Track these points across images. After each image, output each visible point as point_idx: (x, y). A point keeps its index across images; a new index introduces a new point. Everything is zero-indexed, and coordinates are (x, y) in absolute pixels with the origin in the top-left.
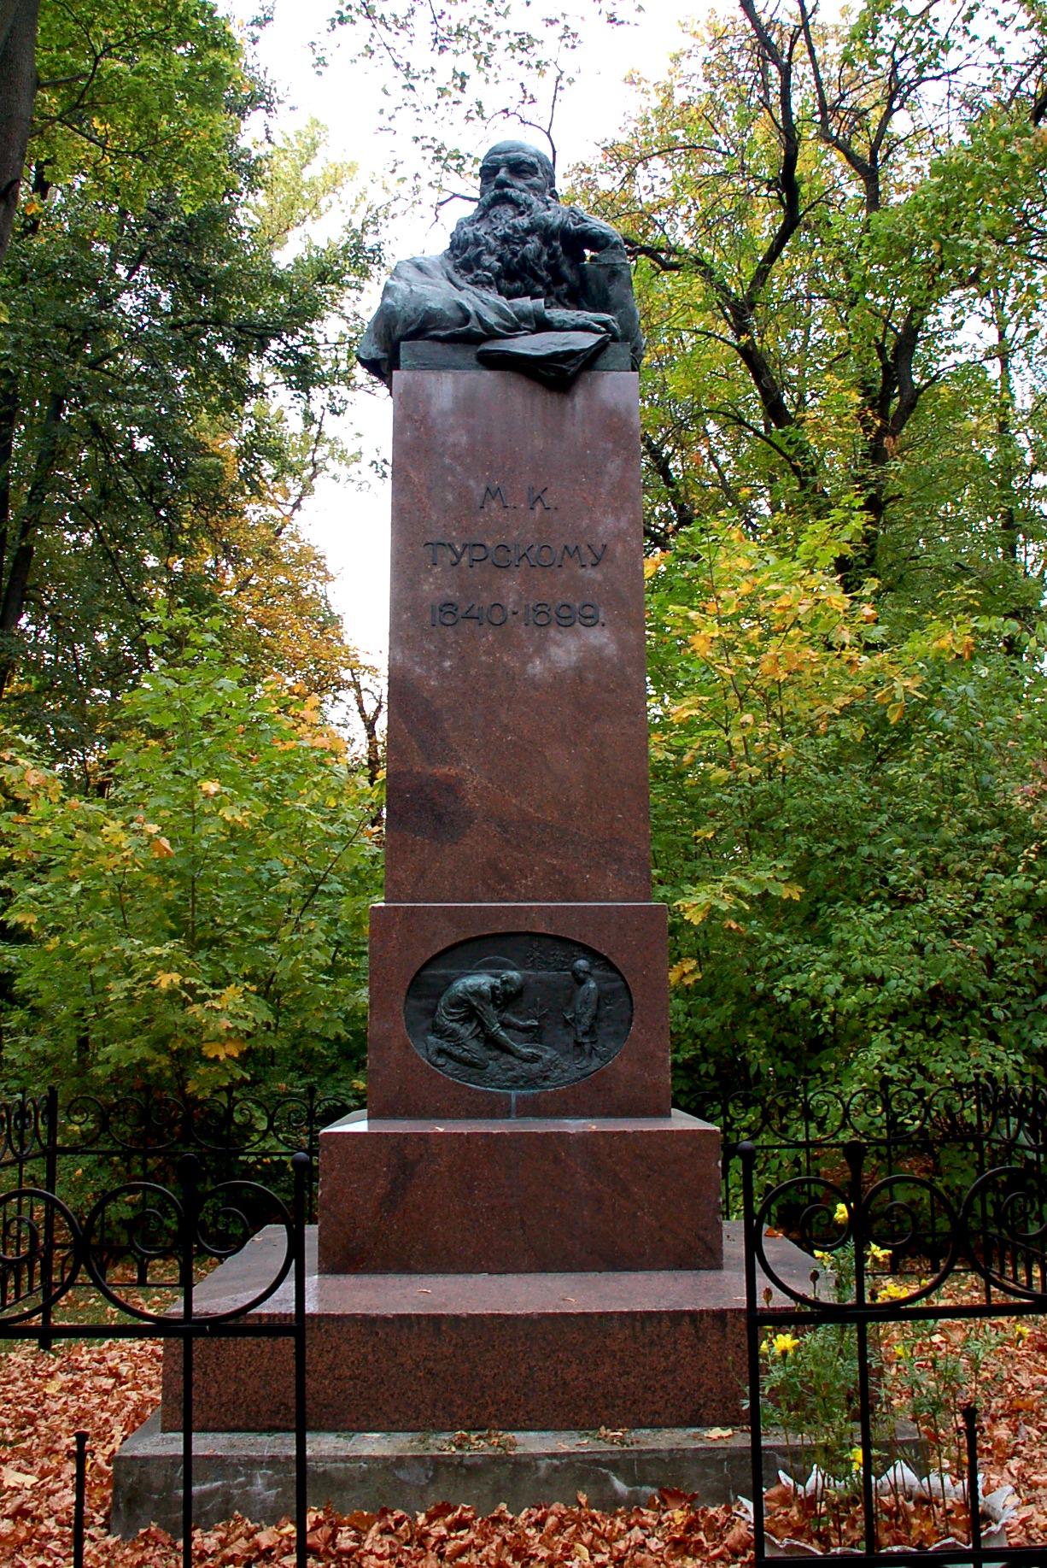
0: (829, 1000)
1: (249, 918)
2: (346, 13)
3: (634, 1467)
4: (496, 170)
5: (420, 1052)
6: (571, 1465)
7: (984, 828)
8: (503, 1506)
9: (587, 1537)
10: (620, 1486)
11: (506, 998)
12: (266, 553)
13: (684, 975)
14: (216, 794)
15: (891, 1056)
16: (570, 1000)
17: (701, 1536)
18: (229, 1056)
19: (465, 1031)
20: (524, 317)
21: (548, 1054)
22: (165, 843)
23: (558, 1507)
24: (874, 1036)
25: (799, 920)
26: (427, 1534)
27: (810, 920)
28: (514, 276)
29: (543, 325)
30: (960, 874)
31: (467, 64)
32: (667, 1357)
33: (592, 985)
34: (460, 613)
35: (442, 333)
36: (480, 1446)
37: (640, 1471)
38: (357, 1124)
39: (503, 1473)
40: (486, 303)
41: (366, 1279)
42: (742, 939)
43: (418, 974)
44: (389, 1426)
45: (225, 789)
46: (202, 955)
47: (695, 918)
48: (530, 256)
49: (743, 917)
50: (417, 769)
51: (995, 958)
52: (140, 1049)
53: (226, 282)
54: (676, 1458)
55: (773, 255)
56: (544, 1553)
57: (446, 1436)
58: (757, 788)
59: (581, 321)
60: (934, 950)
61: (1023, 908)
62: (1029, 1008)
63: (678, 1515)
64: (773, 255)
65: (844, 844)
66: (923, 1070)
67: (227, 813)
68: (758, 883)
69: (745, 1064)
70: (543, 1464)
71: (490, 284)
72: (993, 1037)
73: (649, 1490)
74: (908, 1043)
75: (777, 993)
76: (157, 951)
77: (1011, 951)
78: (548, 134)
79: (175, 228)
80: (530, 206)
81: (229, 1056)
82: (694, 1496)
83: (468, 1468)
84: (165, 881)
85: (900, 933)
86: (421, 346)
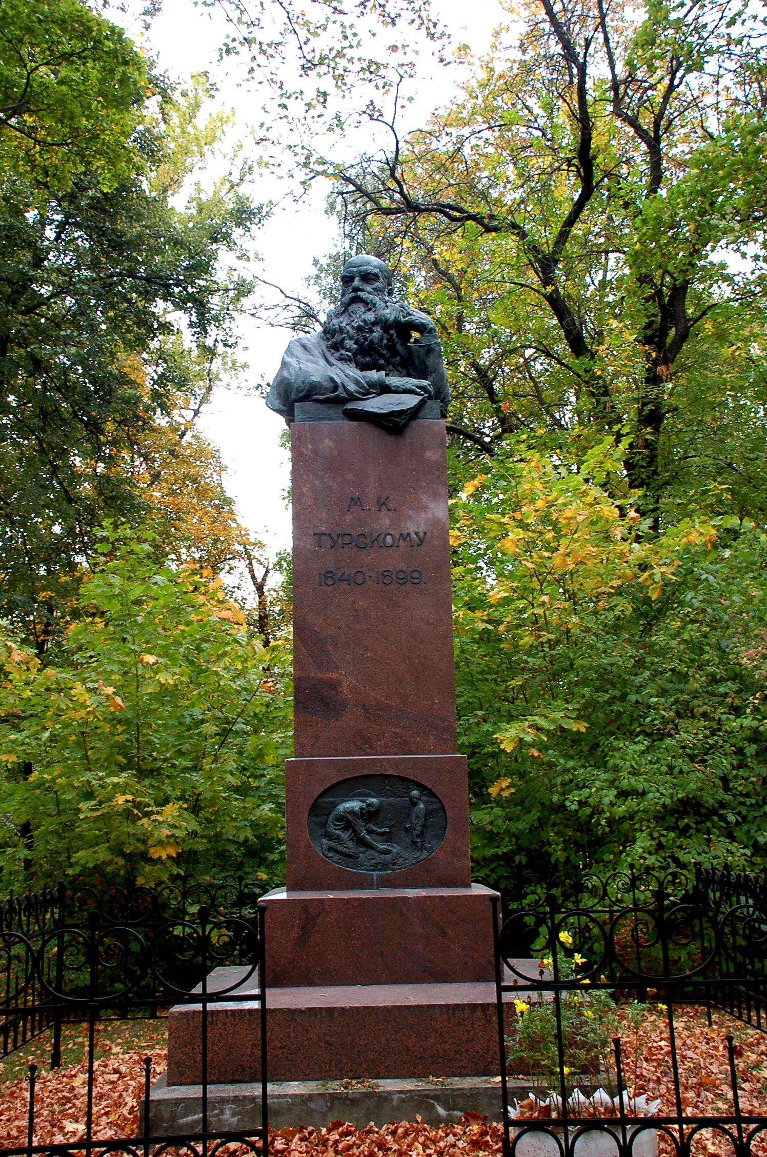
0: (606, 809)
1: (180, 753)
2: (231, 45)
3: (449, 1099)
4: (352, 279)
5: (318, 849)
6: (412, 1097)
7: (722, 680)
8: (372, 1123)
9: (421, 1139)
10: (441, 1111)
11: (369, 815)
12: (173, 453)
13: (502, 790)
14: (154, 664)
15: (652, 849)
16: (409, 815)
17: (488, 1138)
18: (169, 857)
19: (345, 836)
20: (372, 385)
21: (396, 849)
22: (118, 700)
23: (405, 1123)
24: (638, 834)
25: (586, 749)
26: (328, 1139)
27: (589, 748)
28: (366, 355)
29: (385, 389)
30: (704, 715)
31: (327, 84)
32: (468, 1032)
33: (422, 806)
34: (336, 578)
35: (321, 397)
36: (358, 1087)
37: (454, 1101)
38: (281, 895)
39: (371, 1103)
40: (347, 375)
41: (287, 990)
42: (543, 764)
43: (316, 801)
44: (304, 1077)
45: (160, 660)
46: (147, 782)
47: (508, 747)
48: (376, 341)
49: (543, 748)
50: (312, 675)
51: (730, 777)
52: (102, 854)
53: (135, 244)
54: (474, 1094)
55: (571, 221)
56: (395, 1147)
57: (338, 1082)
58: (554, 652)
59: (409, 386)
60: (681, 772)
61: (751, 740)
62: (756, 814)
63: (475, 1128)
64: (571, 221)
65: (617, 693)
66: (676, 860)
67: (162, 678)
68: (553, 721)
69: (548, 855)
70: (395, 1097)
71: (350, 360)
72: (731, 837)
73: (458, 1113)
74: (663, 839)
75: (568, 803)
76: (116, 780)
77: (741, 772)
78: (392, 128)
79: (92, 198)
80: (374, 305)
81: (169, 857)
82: (485, 1118)
83: (351, 1100)
84: (114, 726)
85: (659, 758)
86: (308, 405)
